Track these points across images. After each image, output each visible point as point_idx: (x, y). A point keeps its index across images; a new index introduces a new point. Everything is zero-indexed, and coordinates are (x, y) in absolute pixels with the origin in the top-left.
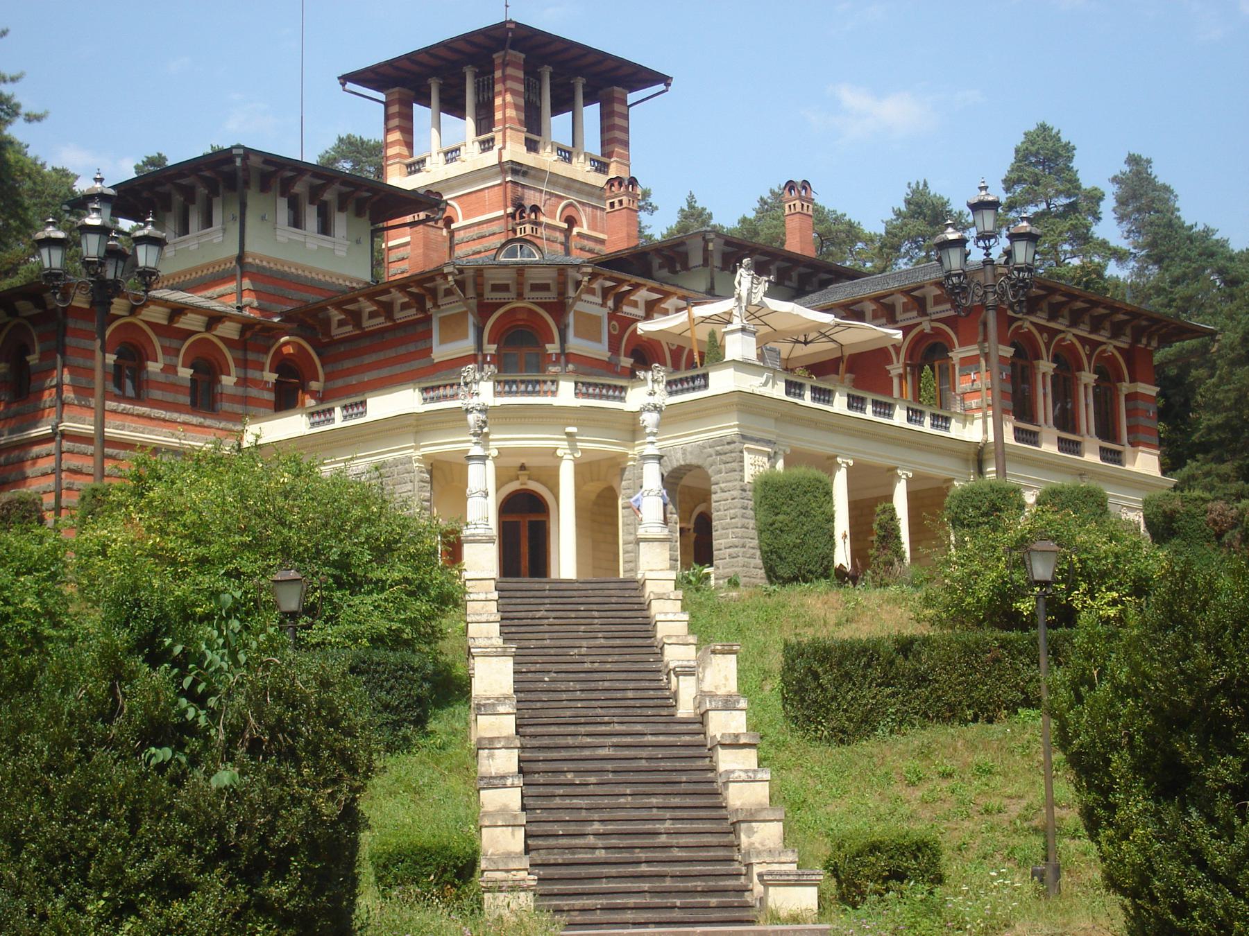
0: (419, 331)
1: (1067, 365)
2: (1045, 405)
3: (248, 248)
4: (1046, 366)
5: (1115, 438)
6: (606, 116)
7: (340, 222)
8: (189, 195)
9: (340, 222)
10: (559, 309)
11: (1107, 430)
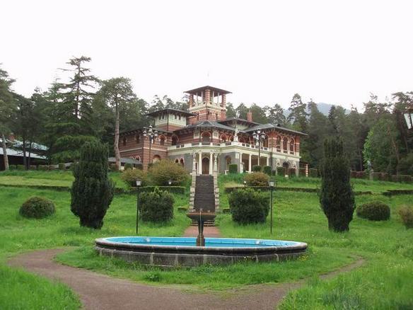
0: (192, 134)
1: (286, 140)
2: (282, 145)
3: (273, 216)
4: (282, 141)
5: (292, 150)
6: (223, 98)
7: (182, 118)
8: (161, 114)
9: (182, 118)
10: (211, 132)
11: (291, 149)
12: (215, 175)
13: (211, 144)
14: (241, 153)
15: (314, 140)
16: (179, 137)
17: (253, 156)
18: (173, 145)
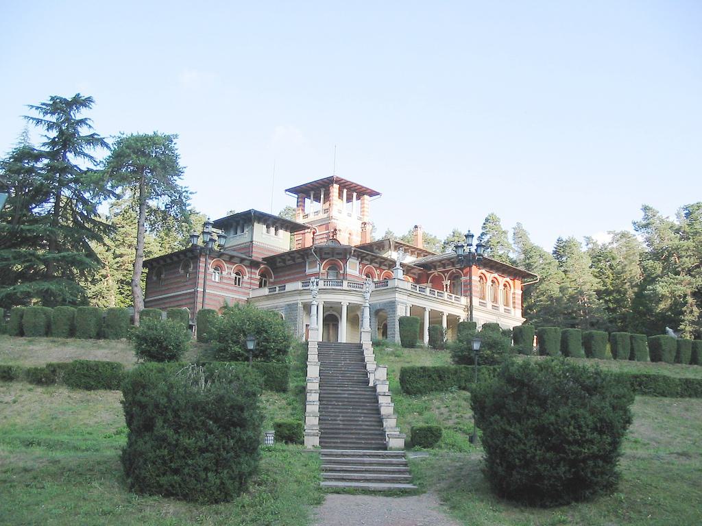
10: (345, 260)
12: (251, 461)
13: (345, 283)
14: (409, 305)
15: (162, 518)
16: (279, 268)
17: (449, 316)
18: (260, 286)
